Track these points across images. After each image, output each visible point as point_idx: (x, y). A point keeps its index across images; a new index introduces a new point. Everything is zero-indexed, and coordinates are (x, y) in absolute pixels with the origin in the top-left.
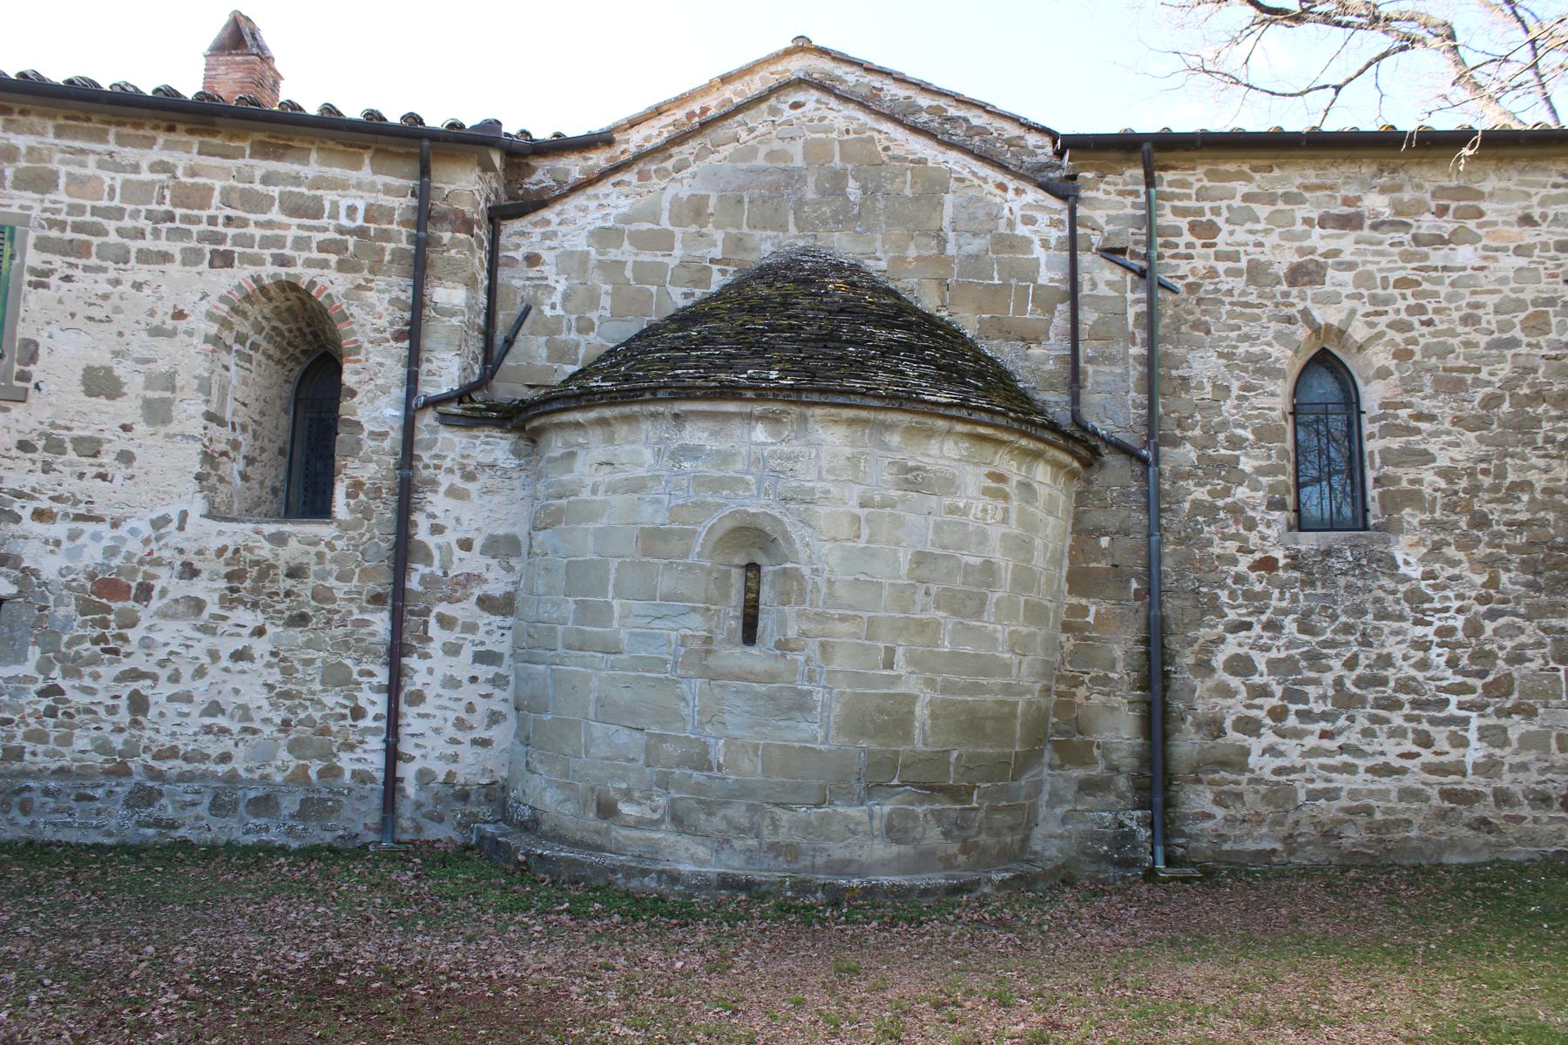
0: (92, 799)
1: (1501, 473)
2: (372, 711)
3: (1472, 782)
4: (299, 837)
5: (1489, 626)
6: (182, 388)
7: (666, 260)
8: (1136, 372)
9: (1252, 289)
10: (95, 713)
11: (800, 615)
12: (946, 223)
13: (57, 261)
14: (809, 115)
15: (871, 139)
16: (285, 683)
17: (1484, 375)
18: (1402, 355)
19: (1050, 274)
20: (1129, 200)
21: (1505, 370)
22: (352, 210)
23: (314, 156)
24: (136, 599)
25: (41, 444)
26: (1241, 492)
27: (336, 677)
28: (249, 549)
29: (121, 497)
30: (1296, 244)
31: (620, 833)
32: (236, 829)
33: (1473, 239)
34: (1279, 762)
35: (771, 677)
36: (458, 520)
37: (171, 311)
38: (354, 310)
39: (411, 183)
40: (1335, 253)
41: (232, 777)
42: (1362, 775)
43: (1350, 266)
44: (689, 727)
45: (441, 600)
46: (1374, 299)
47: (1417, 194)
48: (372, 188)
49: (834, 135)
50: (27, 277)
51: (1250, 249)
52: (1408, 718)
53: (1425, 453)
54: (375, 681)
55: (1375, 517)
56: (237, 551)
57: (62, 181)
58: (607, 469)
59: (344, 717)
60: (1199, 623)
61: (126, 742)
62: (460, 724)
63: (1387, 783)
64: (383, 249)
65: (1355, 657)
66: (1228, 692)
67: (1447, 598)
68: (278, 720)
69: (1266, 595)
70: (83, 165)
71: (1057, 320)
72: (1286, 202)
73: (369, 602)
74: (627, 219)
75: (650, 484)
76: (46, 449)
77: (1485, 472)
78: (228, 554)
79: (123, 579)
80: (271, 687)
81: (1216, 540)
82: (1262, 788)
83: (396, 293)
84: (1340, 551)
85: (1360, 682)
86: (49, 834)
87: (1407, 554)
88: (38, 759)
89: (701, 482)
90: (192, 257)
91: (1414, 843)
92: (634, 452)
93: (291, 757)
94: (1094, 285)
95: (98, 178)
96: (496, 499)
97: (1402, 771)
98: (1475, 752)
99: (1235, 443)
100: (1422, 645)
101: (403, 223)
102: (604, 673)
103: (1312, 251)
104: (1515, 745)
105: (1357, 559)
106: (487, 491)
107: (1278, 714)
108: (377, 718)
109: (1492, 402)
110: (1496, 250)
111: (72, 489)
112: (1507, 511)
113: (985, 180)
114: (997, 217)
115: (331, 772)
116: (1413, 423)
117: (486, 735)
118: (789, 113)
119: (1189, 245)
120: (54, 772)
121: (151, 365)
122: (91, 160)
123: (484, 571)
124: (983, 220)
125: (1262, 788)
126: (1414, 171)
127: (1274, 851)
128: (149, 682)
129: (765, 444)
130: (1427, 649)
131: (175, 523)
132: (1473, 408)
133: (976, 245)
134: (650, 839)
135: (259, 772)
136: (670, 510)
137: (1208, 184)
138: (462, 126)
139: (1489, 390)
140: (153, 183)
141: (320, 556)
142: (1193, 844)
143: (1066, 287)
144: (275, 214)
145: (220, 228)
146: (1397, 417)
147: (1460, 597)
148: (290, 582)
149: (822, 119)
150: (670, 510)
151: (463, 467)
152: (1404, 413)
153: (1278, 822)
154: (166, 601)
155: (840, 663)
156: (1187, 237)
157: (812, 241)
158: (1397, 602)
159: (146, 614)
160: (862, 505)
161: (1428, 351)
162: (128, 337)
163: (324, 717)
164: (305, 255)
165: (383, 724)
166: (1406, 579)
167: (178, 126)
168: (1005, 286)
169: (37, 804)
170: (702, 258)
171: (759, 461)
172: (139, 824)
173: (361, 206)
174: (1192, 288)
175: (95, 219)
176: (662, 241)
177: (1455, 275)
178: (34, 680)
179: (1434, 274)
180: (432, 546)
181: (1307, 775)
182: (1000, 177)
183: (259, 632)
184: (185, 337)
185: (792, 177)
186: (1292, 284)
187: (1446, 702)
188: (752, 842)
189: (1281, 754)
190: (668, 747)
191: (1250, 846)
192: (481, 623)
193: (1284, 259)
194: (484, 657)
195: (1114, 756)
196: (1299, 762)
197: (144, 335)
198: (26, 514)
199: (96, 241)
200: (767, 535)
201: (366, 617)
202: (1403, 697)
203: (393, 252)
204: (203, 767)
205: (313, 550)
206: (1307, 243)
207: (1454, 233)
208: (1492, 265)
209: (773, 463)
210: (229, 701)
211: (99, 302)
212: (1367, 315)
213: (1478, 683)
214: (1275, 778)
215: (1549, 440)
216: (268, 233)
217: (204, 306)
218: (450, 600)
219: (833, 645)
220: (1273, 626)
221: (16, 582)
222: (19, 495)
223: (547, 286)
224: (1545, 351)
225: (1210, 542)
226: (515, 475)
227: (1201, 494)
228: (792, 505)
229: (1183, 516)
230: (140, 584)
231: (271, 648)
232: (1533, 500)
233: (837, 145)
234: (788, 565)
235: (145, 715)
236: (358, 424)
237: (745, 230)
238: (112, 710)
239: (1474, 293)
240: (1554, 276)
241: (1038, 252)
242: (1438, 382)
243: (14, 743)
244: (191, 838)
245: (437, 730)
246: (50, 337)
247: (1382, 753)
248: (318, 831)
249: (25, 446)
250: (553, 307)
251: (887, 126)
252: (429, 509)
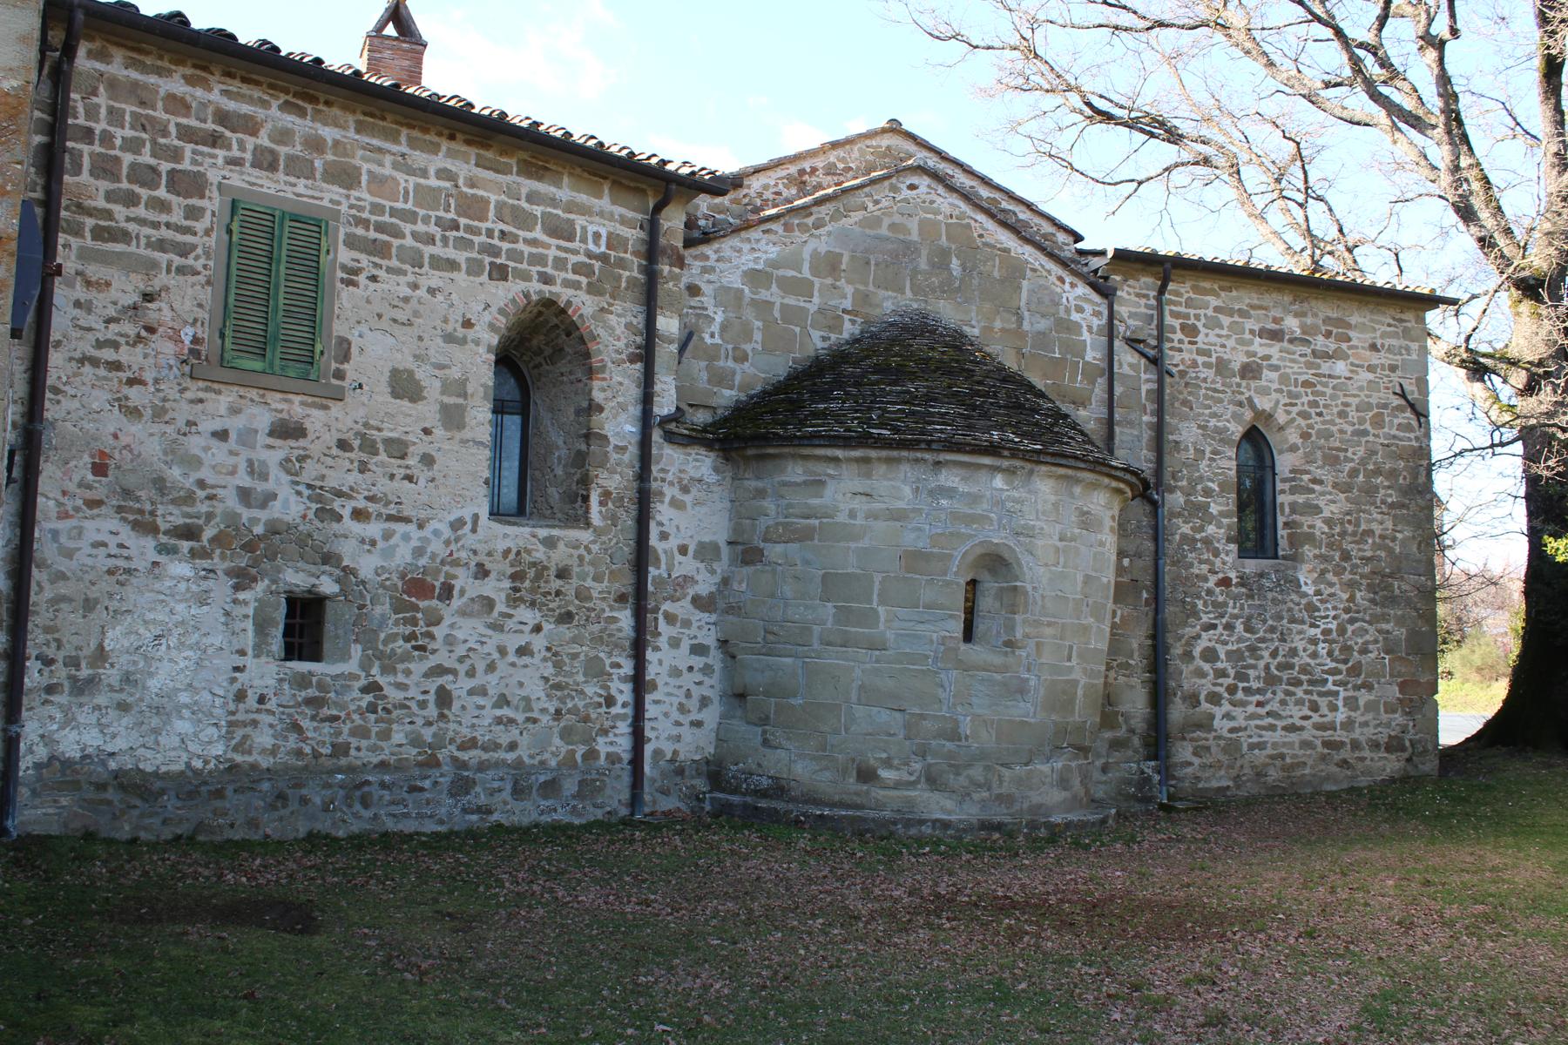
0: (422, 789)
1: (1357, 525)
2: (620, 699)
3: (1340, 735)
4: (580, 815)
5: (1350, 628)
6: (472, 395)
7: (807, 305)
8: (1147, 434)
9: (1218, 379)
10: (408, 708)
11: (1024, 622)
12: (1023, 304)
13: (365, 260)
14: (923, 197)
15: (968, 226)
16: (556, 675)
17: (1349, 454)
18: (1305, 436)
19: (1093, 355)
20: (1143, 301)
21: (1361, 451)
22: (597, 236)
23: (566, 179)
24: (440, 598)
25: (356, 443)
26: (1211, 529)
27: (595, 670)
28: (529, 552)
29: (424, 498)
30: (1245, 348)
31: (879, 794)
32: (525, 812)
33: (1345, 357)
34: (1233, 724)
35: (1003, 669)
36: (678, 528)
37: (461, 320)
38: (600, 331)
39: (640, 216)
40: (1267, 357)
41: (519, 763)
42: (1279, 732)
43: (1276, 368)
44: (945, 708)
45: (665, 599)
46: (1290, 395)
47: (1314, 320)
48: (611, 217)
49: (940, 218)
50: (340, 274)
51: (1218, 349)
52: (1306, 692)
53: (1317, 507)
54: (622, 671)
55: (1284, 550)
56: (518, 553)
57: (364, 178)
58: (864, 498)
59: (600, 705)
60: (1185, 624)
61: (435, 735)
62: (682, 709)
63: (1294, 737)
64: (620, 276)
65: (1277, 649)
66: (1202, 675)
67: (1327, 609)
68: (552, 710)
69: (1225, 604)
70: (381, 164)
71: (1097, 390)
72: (1240, 316)
73: (615, 601)
74: (775, 264)
75: (911, 515)
76: (361, 448)
77: (1349, 522)
78: (512, 556)
79: (429, 579)
80: (546, 679)
81: (1196, 564)
82: (1222, 743)
83: (629, 318)
84: (1268, 574)
85: (1280, 667)
86: (391, 825)
87: (1306, 577)
88: (361, 754)
89: (956, 516)
90: (474, 268)
91: (1308, 778)
92: (894, 487)
93: (562, 743)
94: (1121, 365)
95: (394, 179)
96: (704, 510)
97: (1301, 729)
98: (1341, 715)
99: (1208, 492)
100: (1314, 641)
101: (634, 253)
102: (868, 666)
103: (1255, 354)
104: (1362, 709)
105: (1278, 581)
106: (697, 503)
107: (1232, 690)
108: (624, 705)
109: (1354, 473)
110: (1357, 366)
111: (383, 489)
112: (1360, 550)
113: (1049, 272)
114: (1058, 304)
115: (591, 755)
116: (1311, 485)
117: (699, 717)
118: (906, 193)
119: (1180, 341)
120: (376, 766)
121: (447, 371)
122: (388, 159)
123: (695, 573)
124: (1048, 304)
125: (1222, 743)
126: (1313, 303)
127: (1228, 787)
128: (450, 677)
129: (1002, 490)
130: (1316, 644)
131: (469, 526)
132: (1343, 477)
133: (1043, 324)
134: (906, 797)
135: (538, 758)
136: (931, 537)
137: (1193, 296)
138: (186, 23)
139: (1352, 464)
140: (439, 189)
141: (581, 558)
142: (1181, 785)
143: (1105, 365)
144: (538, 233)
145: (496, 242)
146: (1301, 480)
147: (1335, 608)
148: (559, 582)
149: (932, 202)
150: (931, 537)
151: (680, 480)
152: (1306, 477)
153: (1231, 767)
154: (464, 600)
155: (1046, 658)
156: (1179, 335)
157: (923, 305)
158: (1300, 611)
159: (448, 611)
160: (1061, 540)
161: (1320, 434)
162: (427, 342)
163: (586, 706)
164: (563, 275)
165: (629, 711)
166: (1305, 595)
167: (459, 136)
168: (1063, 359)
169: (376, 797)
170: (837, 308)
171: (1000, 503)
172: (465, 811)
173: (604, 232)
174: (1183, 374)
175: (393, 220)
176: (803, 288)
177: (1335, 381)
178: (357, 678)
179: (1324, 380)
180: (660, 551)
181: (1248, 733)
183: (537, 629)
184: (472, 345)
185: (908, 248)
186: (1243, 378)
187: (1326, 681)
188: (986, 794)
189: (1234, 718)
190: (927, 724)
191: (1215, 784)
192: (694, 619)
193: (1238, 360)
194: (699, 650)
195: (1132, 722)
196: (1244, 724)
197: (439, 341)
198: (346, 513)
199: (396, 242)
200: (1004, 560)
201: (615, 614)
202: (1303, 677)
203: (629, 280)
204: (496, 755)
205: (576, 553)
206: (1251, 348)
207: (1335, 351)
208: (1355, 377)
209: (1009, 505)
210: (515, 694)
211: (401, 304)
212: (1285, 405)
213: (1343, 667)
214: (1229, 735)
215: (1383, 502)
216: (534, 250)
217: (487, 317)
218: (674, 599)
219: (1043, 643)
220: (1229, 627)
221: (338, 581)
222: (339, 494)
223: (707, 316)
224: (1382, 441)
225: (1191, 566)
226: (715, 489)
227: (1186, 529)
228: (1021, 539)
229: (1175, 545)
230: (443, 584)
231: (546, 644)
232: (1374, 543)
233: (943, 225)
234: (1018, 584)
235: (450, 709)
236: (605, 438)
237: (871, 288)
238: (423, 705)
239: (1345, 395)
240: (1387, 388)
241: (1086, 336)
242: (1325, 457)
243: (340, 740)
244: (503, 821)
245: (666, 715)
246: (360, 336)
247: (1291, 717)
248: (590, 809)
249: (343, 445)
250: (712, 336)
251: (981, 217)
252: (658, 517)
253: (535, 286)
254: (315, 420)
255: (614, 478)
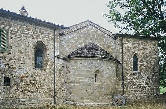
18: (142, 56)
19: (114, 47)
26: (129, 68)
63: (140, 93)
90: (29, 37)
98: (147, 90)
107: (132, 87)
109: (148, 60)
176: (76, 40)
182: (110, 37)
199: (18, 34)
227: (126, 68)
253: (39, 40)
254: (7, 56)
255: (51, 63)
